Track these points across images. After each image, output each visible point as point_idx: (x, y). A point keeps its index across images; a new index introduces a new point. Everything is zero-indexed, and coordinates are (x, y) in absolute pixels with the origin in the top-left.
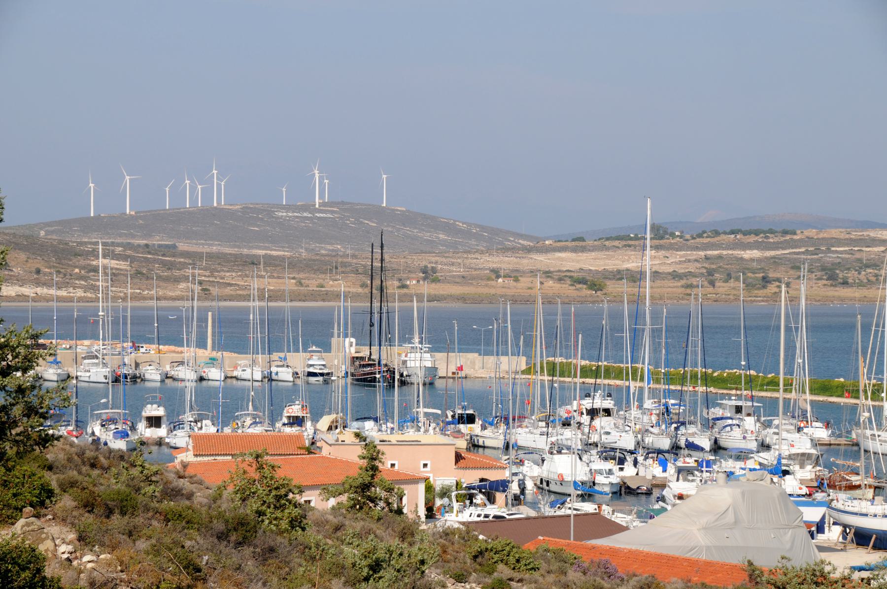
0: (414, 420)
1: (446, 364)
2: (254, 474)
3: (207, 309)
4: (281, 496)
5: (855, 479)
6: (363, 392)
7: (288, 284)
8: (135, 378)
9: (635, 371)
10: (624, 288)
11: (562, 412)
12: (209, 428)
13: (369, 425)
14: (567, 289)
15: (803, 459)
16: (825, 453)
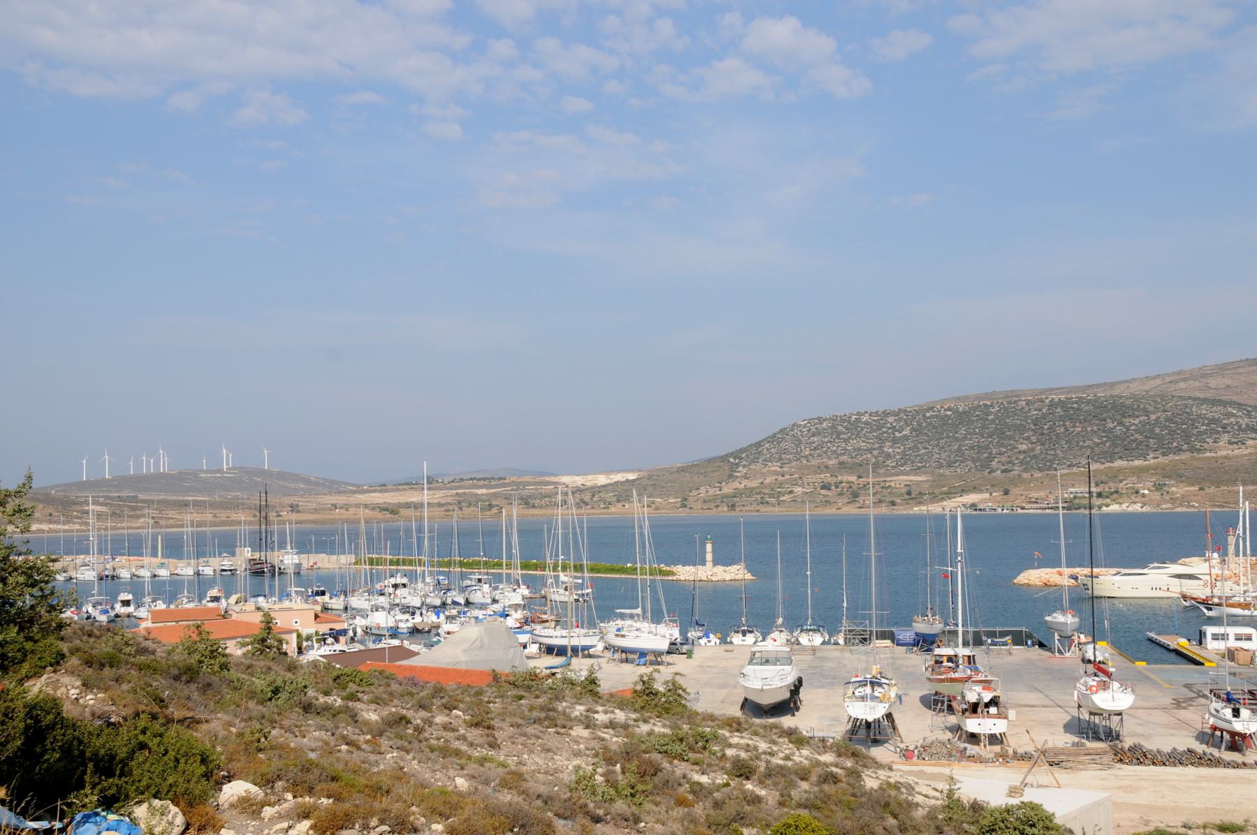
0: (288, 595)
1: (307, 561)
2: (195, 637)
3: (157, 534)
4: (214, 653)
5: (545, 617)
6: (257, 580)
7: (209, 517)
8: (113, 577)
9: (420, 561)
10: (411, 513)
11: (378, 586)
12: (161, 606)
13: (261, 599)
14: (377, 514)
15: (516, 607)
16: (528, 604)
